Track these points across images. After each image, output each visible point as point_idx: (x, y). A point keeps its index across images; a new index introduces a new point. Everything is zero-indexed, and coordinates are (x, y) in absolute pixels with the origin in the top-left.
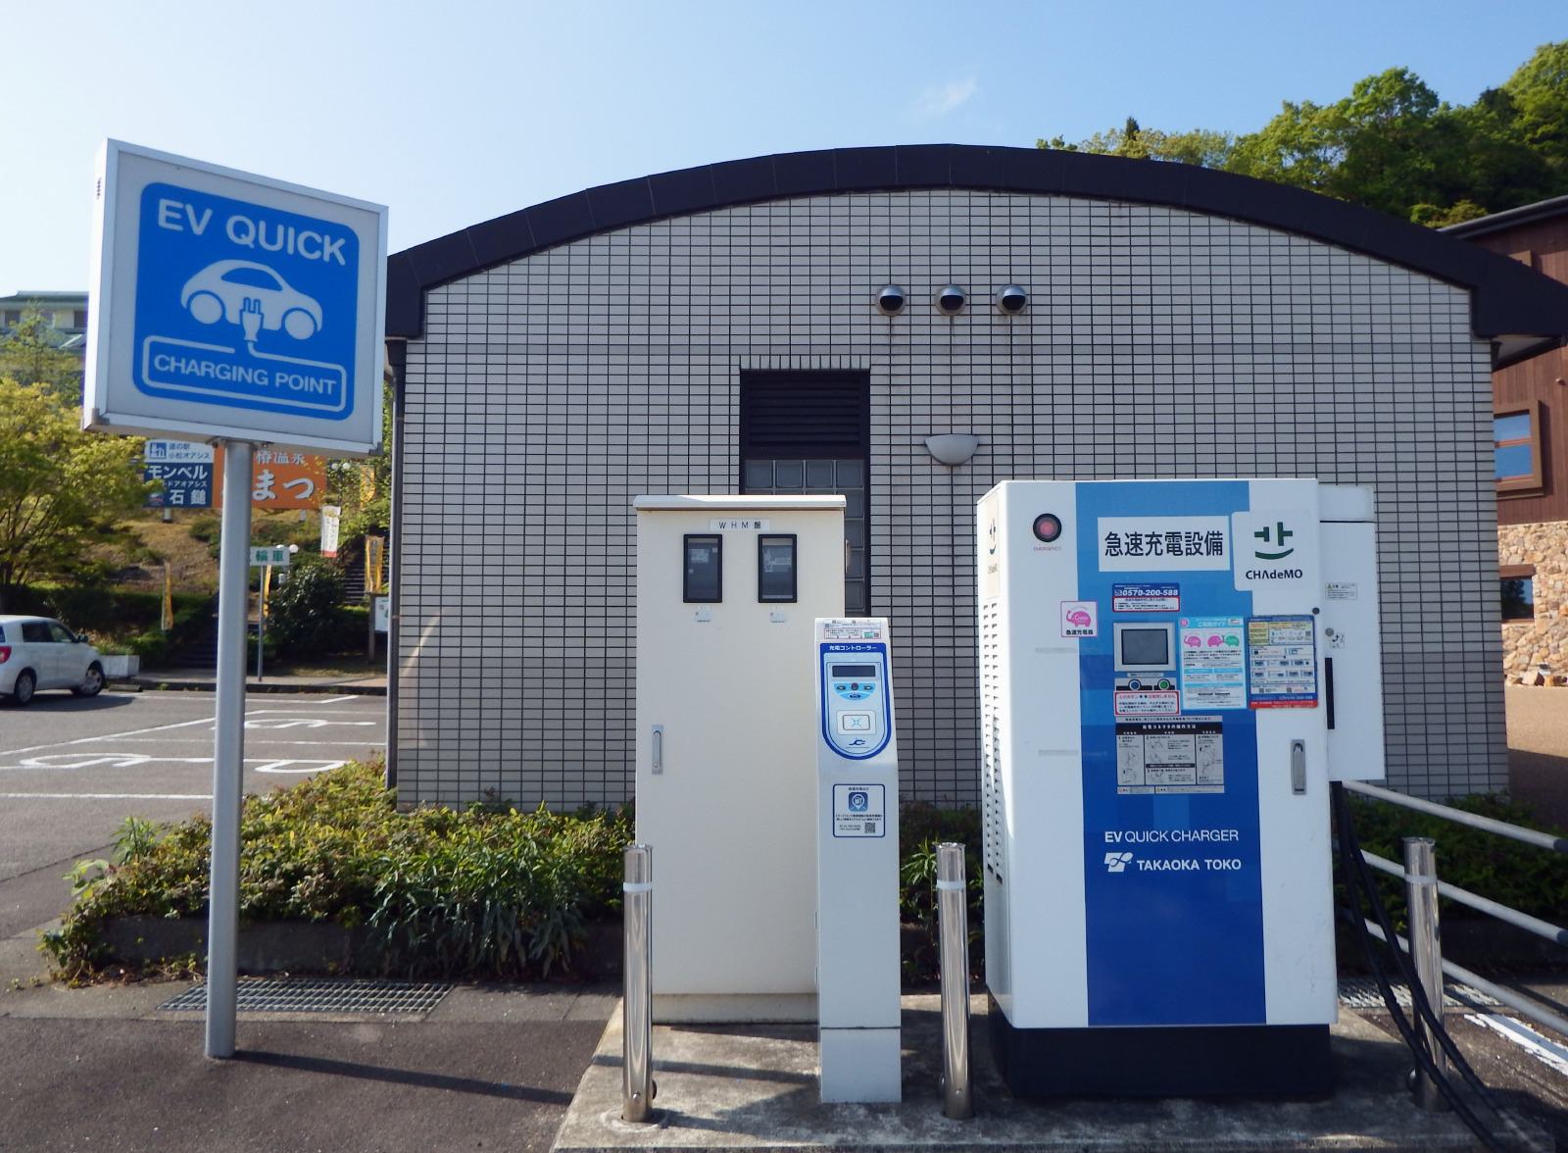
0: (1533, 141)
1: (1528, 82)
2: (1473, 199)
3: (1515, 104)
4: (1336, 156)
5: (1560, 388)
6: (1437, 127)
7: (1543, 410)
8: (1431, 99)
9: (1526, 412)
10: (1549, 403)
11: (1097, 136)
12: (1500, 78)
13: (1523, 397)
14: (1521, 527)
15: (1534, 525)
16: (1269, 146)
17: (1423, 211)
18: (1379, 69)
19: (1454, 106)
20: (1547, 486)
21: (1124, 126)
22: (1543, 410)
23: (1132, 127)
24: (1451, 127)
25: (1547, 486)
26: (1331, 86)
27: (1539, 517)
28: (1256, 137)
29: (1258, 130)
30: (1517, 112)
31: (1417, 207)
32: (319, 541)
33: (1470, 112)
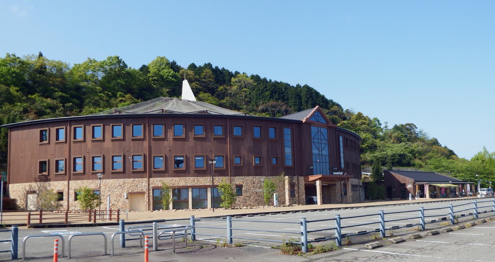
0: (152, 80)
1: (154, 64)
2: (132, 94)
3: (149, 70)
4: (100, 75)
5: (87, 153)
6: (126, 73)
7: (84, 157)
8: (126, 66)
9: (81, 157)
10: (85, 156)
11: (29, 55)
12: (147, 62)
13: (81, 155)
14: (80, 181)
15: (82, 181)
16: (82, 68)
17: (120, 94)
18: (113, 55)
19: (132, 68)
20: (124, 172)
21: (38, 54)
22: (84, 157)
23: (41, 55)
24: (130, 75)
25: (124, 172)
26: (101, 57)
27: (83, 179)
28: (79, 65)
29: (81, 63)
30: (149, 72)
31: (119, 93)
32: (152, 178)
33: (136, 71)
